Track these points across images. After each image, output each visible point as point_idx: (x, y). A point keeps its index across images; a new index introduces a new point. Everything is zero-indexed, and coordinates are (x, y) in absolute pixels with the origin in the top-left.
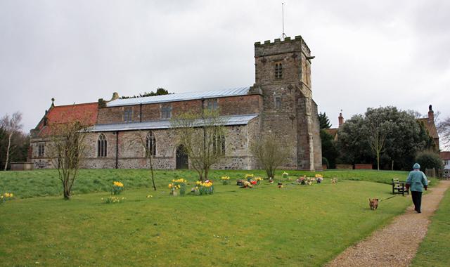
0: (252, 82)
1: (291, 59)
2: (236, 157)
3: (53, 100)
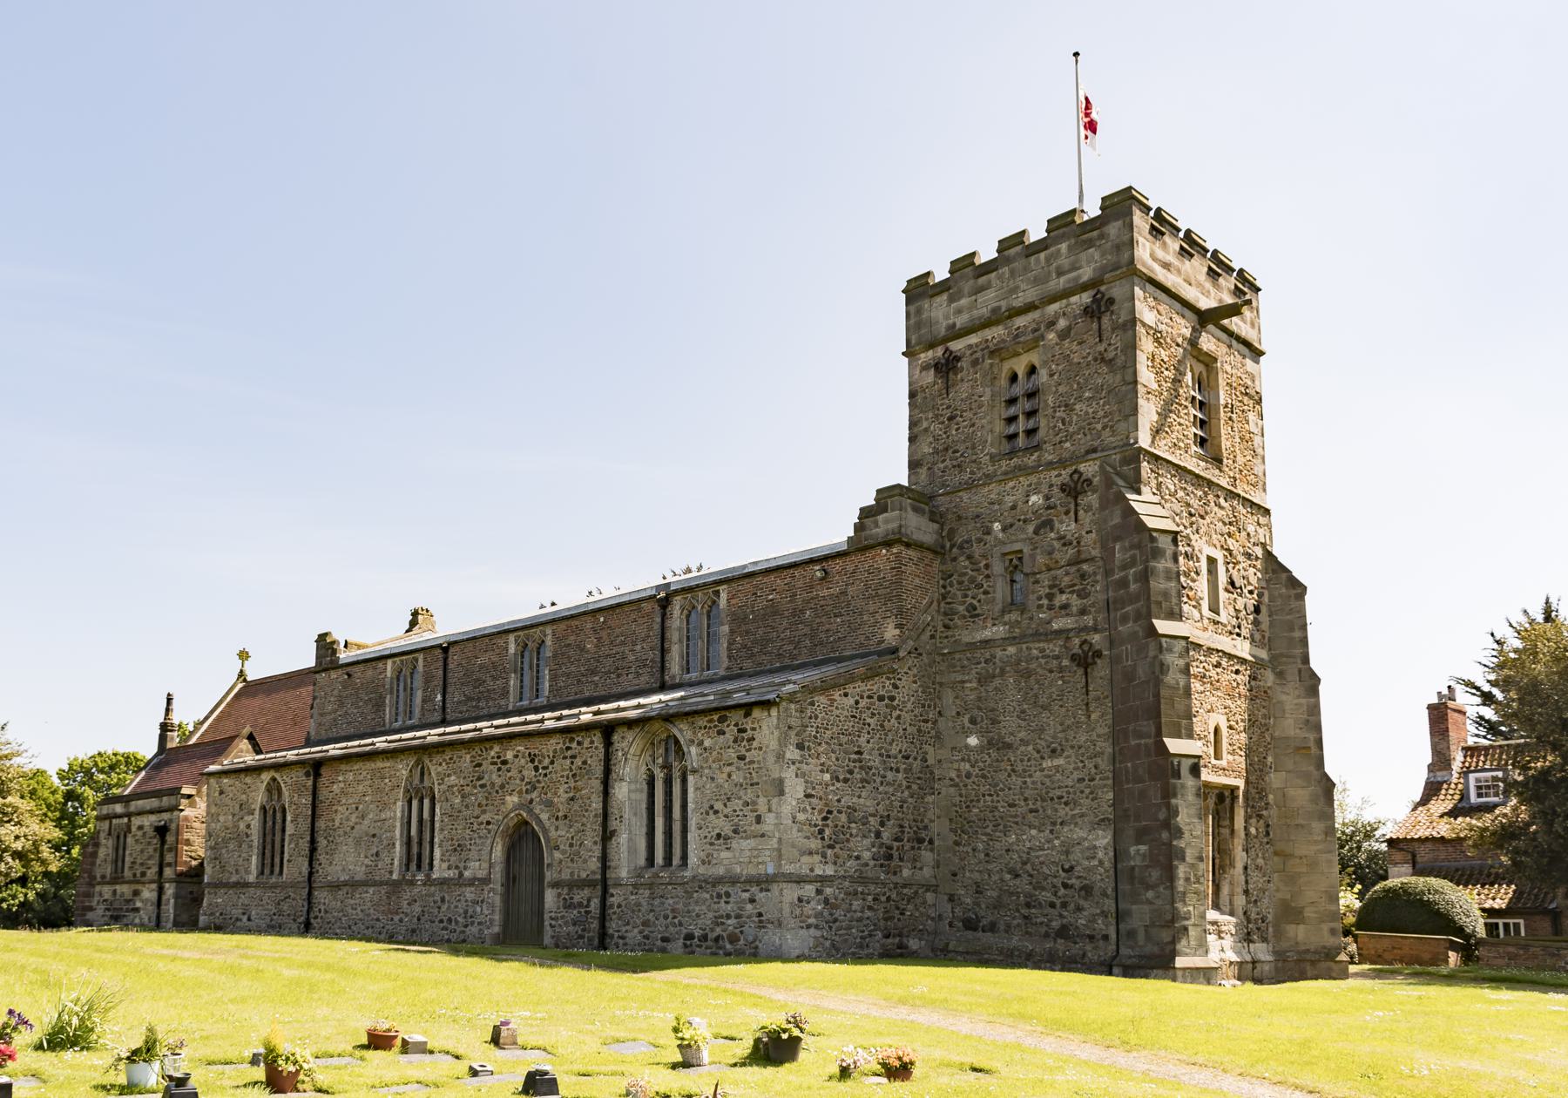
2: (734, 880)
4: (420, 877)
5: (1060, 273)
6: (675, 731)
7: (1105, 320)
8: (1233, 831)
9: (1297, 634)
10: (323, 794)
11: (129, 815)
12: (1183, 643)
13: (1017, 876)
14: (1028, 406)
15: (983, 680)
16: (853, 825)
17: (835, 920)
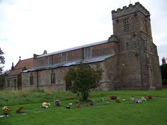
0: (111, 32)
1: (134, 17)
3: (20, 57)
4: (54, 84)
5: (131, 11)
6: (90, 65)
9: (156, 52)
10: (39, 74)
11: (10, 78)
13: (130, 80)
14: (128, 26)
15: (124, 58)
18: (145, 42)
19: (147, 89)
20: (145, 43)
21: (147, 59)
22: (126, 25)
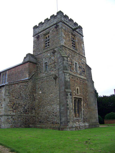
5: (52, 23)
7: (58, 28)
8: (81, 105)
12: (69, 74)
13: (46, 114)
16: (19, 106)
17: (15, 122)
18: (66, 58)
19: (65, 127)
20: (64, 60)
21: (66, 82)
22: (46, 41)
